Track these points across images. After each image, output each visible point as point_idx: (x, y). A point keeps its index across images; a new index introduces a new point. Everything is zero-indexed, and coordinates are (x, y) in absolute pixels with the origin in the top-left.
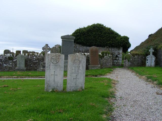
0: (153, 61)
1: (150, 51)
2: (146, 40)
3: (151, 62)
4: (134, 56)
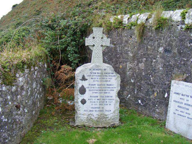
0: (114, 94)
1: (88, 41)
2: (9, 13)
3: (102, 101)
4: (10, 84)
